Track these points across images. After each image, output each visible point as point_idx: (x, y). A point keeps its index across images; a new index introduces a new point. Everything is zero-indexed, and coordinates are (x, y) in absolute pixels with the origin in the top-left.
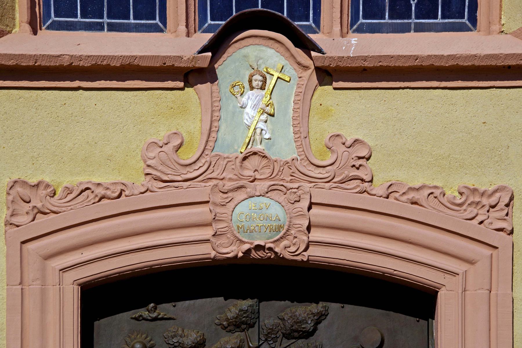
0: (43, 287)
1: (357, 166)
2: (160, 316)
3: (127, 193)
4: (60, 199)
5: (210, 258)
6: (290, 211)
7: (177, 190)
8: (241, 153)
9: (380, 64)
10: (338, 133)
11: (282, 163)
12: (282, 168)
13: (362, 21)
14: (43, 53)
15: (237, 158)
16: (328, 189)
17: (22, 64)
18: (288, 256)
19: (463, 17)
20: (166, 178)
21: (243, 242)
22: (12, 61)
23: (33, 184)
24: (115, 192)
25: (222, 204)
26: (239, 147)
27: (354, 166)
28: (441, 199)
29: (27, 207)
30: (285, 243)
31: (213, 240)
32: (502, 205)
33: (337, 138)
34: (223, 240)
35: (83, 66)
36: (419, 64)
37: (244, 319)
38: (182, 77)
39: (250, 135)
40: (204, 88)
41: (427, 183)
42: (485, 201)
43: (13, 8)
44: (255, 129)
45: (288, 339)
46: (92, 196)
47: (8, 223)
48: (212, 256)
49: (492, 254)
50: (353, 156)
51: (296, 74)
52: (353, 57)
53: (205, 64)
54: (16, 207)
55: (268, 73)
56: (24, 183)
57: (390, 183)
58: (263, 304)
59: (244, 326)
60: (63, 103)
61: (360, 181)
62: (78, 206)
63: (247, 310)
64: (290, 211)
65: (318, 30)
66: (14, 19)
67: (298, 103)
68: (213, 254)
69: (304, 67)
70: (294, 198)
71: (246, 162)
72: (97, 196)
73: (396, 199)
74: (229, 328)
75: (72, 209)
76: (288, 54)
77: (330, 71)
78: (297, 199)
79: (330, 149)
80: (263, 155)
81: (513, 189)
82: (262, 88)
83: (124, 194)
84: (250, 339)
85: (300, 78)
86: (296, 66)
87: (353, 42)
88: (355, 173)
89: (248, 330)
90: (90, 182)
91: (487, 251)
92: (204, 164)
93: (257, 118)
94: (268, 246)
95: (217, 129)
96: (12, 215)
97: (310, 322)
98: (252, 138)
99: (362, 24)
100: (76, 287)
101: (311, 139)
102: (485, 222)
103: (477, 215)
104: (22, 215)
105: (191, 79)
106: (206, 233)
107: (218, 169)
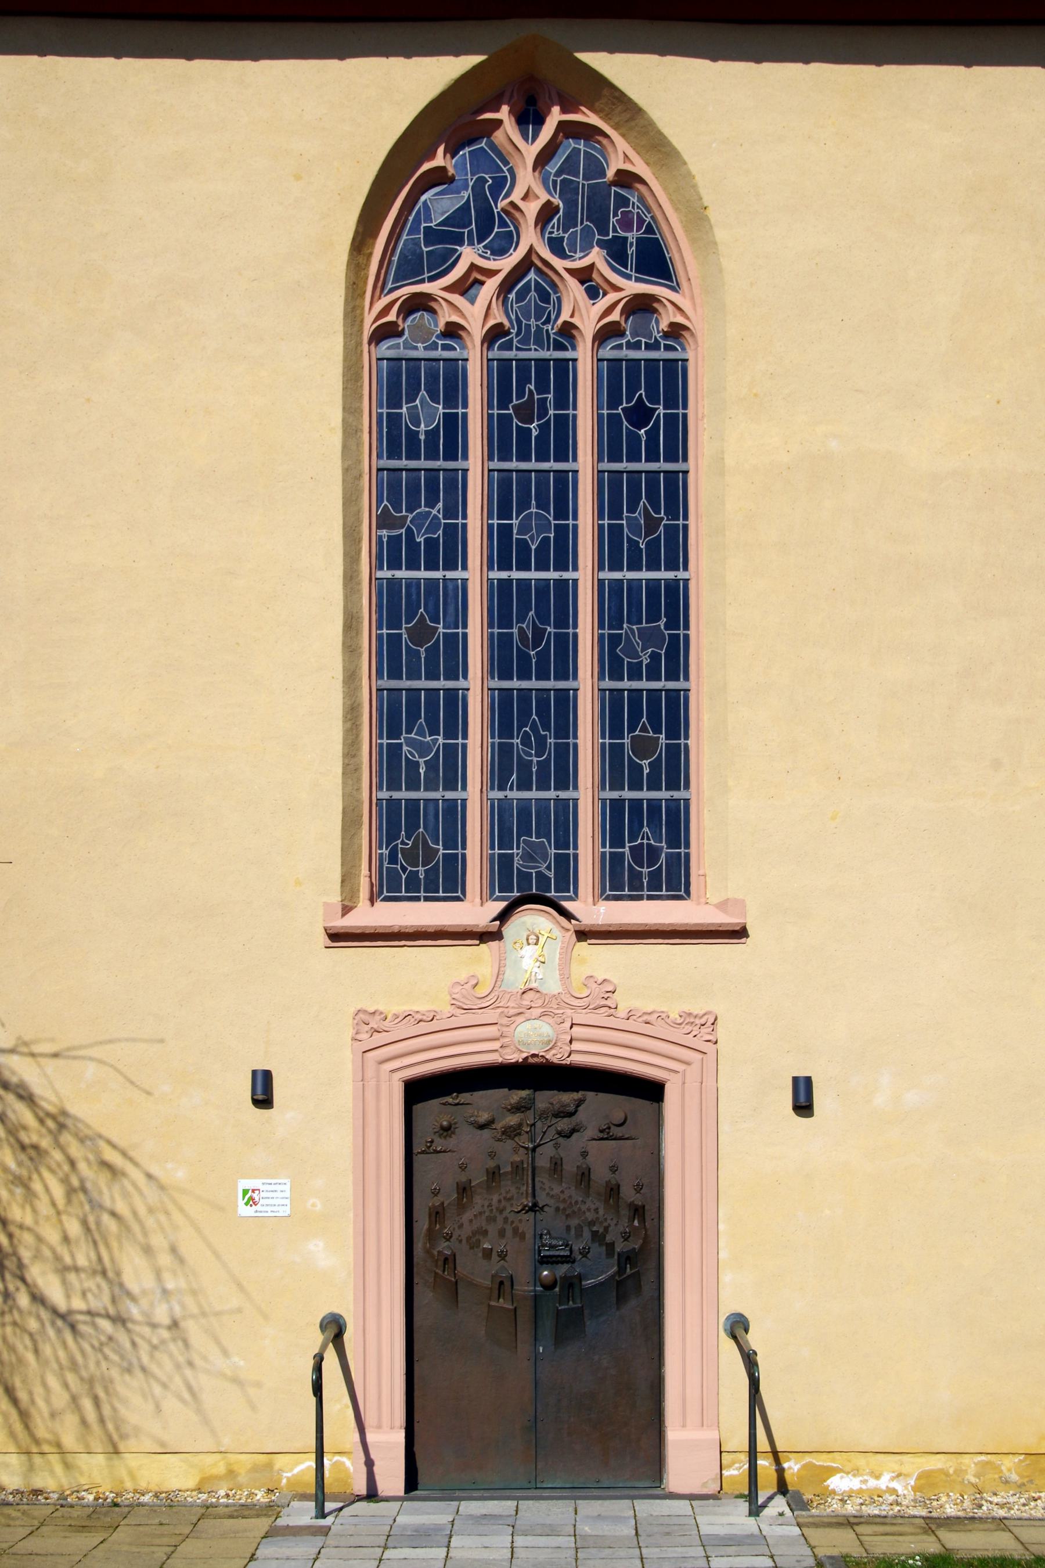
3: (438, 1017)
18: (555, 1061)
20: (466, 1007)
28: (667, 1020)
29: (367, 1028)
30: (553, 1052)
31: (500, 1050)
32: (709, 1024)
34: (507, 1050)
39: (527, 977)
40: (494, 944)
42: (698, 1021)
43: (358, 890)
45: (557, 1118)
46: (413, 1020)
47: (354, 1039)
49: (703, 1058)
53: (495, 929)
56: (365, 1012)
58: (537, 1093)
66: (359, 897)
68: (500, 1060)
70: (560, 1020)
71: (524, 995)
73: (635, 1020)
74: (512, 1111)
76: (554, 921)
81: (717, 1012)
82: (536, 944)
83: (435, 1018)
86: (560, 929)
87: (602, 911)
88: (604, 1002)
91: (699, 1056)
94: (540, 1054)
96: (357, 1034)
99: (609, 895)
100: (401, 1083)
106: (496, 1045)
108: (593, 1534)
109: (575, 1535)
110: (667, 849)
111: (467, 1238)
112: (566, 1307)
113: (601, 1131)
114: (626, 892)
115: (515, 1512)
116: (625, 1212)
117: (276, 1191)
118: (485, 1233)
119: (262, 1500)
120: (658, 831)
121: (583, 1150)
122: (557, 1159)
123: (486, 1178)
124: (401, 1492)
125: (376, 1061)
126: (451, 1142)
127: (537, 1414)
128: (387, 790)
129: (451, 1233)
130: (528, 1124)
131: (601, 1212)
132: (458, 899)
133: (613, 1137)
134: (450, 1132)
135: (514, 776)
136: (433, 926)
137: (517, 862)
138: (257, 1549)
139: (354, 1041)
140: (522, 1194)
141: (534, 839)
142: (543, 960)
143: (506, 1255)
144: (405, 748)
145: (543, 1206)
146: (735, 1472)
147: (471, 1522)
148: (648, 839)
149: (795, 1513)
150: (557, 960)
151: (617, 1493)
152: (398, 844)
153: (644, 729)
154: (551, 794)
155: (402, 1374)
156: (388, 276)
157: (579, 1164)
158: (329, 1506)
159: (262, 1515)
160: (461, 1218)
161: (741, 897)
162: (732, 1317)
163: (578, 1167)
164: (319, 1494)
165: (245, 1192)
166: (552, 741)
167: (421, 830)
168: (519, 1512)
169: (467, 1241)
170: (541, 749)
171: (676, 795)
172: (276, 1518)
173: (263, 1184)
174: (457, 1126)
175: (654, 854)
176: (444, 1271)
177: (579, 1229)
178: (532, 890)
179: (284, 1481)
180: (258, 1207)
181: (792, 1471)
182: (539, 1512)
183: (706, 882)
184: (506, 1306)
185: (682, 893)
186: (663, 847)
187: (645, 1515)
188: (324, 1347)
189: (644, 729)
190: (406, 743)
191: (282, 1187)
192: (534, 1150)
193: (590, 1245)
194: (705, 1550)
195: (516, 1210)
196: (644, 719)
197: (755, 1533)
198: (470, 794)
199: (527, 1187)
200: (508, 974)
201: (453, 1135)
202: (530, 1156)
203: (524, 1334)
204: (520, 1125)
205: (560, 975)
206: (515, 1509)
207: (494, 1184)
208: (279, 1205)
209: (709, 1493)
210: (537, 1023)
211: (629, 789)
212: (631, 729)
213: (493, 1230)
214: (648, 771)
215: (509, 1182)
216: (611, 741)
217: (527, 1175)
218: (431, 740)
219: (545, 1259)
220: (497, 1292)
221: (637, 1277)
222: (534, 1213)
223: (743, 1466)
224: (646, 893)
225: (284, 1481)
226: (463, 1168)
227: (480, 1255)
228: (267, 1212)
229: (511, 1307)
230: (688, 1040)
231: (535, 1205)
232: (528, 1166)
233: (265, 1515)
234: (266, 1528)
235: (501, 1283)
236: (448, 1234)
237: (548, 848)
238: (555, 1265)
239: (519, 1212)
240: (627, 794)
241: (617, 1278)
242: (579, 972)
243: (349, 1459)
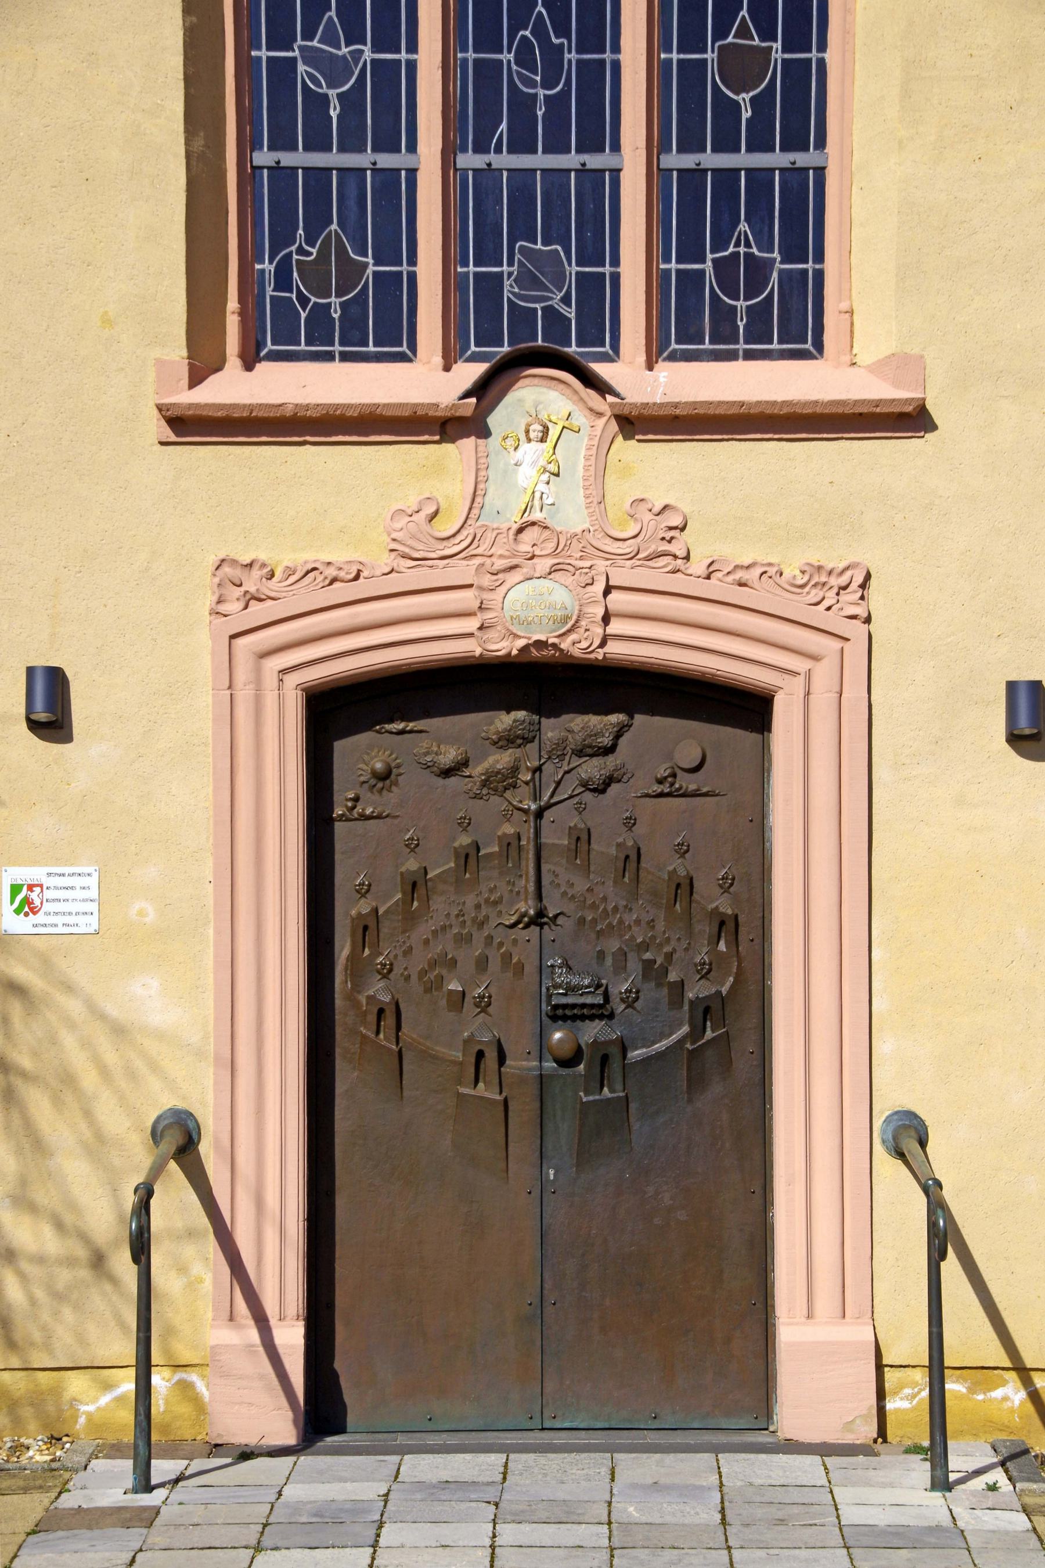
0: (258, 692)
1: (668, 538)
2: (408, 728)
4: (280, 582)
6: (580, 596)
7: (430, 571)
8: (516, 522)
9: (696, 411)
10: (642, 497)
11: (569, 535)
12: (569, 542)
13: (674, 346)
14: (260, 401)
15: (509, 529)
16: (630, 567)
17: (235, 415)
18: (576, 652)
19: (806, 342)
21: (517, 636)
22: (222, 412)
23: (245, 563)
24: (350, 573)
25: (491, 588)
26: (512, 516)
27: (663, 539)
29: (238, 592)
30: (573, 637)
32: (854, 585)
33: (641, 503)
34: (491, 634)
35: (310, 417)
36: (746, 411)
37: (520, 732)
38: (437, 428)
41: (759, 559)
42: (835, 582)
45: (580, 757)
48: (477, 653)
49: (842, 648)
50: (663, 526)
51: (587, 423)
52: (660, 403)
53: (468, 412)
54: (224, 591)
55: (550, 421)
56: (234, 562)
57: (710, 560)
59: (519, 741)
60: (284, 461)
61: (671, 557)
62: (302, 591)
63: (524, 721)
64: (580, 596)
65: (616, 358)
67: (589, 459)
68: (478, 651)
69: (597, 413)
72: (326, 578)
74: (500, 743)
75: (294, 595)
76: (575, 398)
77: (633, 420)
78: (590, 581)
79: (632, 517)
80: (545, 525)
81: (869, 565)
82: (543, 440)
83: (362, 575)
84: (528, 757)
85: (592, 427)
86: (587, 413)
87: (662, 380)
88: (665, 547)
89: (525, 746)
90: (318, 560)
92: (467, 537)
94: (550, 641)
95: (483, 492)
96: (219, 602)
97: (607, 735)
98: (530, 504)
99: (675, 351)
100: (300, 693)
101: (606, 505)
103: (823, 598)
104: (232, 601)
105: (449, 428)
106: (471, 625)
107: (485, 543)
108: (644, 1519)
109: (610, 1523)
110: (781, 263)
111: (420, 973)
112: (597, 1097)
113: (660, 782)
114: (707, 346)
115: (501, 1476)
116: (704, 928)
118: (453, 963)
119: (38, 1458)
120: (766, 229)
121: (628, 814)
122: (581, 830)
123: (452, 865)
124: (289, 1437)
125: (254, 653)
126: (389, 801)
127: (545, 1292)
128: (270, 149)
129: (391, 964)
130: (528, 768)
131: (660, 926)
132: (402, 358)
133: (681, 792)
134: (388, 782)
135: (504, 126)
136: (356, 406)
137: (509, 288)
138: (15, 1556)
139: (214, 616)
140: (518, 893)
141: (539, 246)
142: (555, 470)
143: (489, 1004)
144: (301, 68)
145: (556, 916)
146: (905, 1405)
147: (418, 1496)
148: (748, 245)
149: (1019, 1485)
150: (580, 471)
151: (691, 1438)
152: (292, 252)
153: (743, 32)
154: (571, 160)
157: (620, 840)
158: (162, 1468)
159: (35, 1488)
160: (409, 937)
161: (916, 351)
162: (896, 1117)
163: (619, 845)
164: (141, 1443)
165: (15, 889)
166: (573, 56)
167: (334, 227)
168: (508, 1477)
169: (420, 978)
170: (553, 73)
171: (801, 159)
172: (60, 1493)
173: (49, 874)
174: (401, 771)
175: (758, 271)
176: (378, 1033)
177: (622, 955)
178: (537, 341)
179: (82, 1420)
180: (40, 918)
181: (1009, 1404)
182: (545, 1475)
183: (852, 324)
184: (487, 1095)
185: (809, 346)
186: (775, 260)
187: (739, 1483)
188: (157, 1171)
189: (743, 32)
190: (302, 57)
192: (539, 814)
193: (639, 985)
194: (849, 1555)
195: (507, 923)
196: (744, 12)
197: (944, 1524)
198: (422, 159)
199: (527, 881)
200: (493, 498)
201: (394, 788)
202: (532, 824)
203: (522, 1145)
204: (515, 770)
206: (502, 1469)
207: (468, 875)
208: (77, 914)
209: (858, 1442)
211: (714, 150)
212: (721, 32)
213: (467, 957)
214: (750, 113)
215: (495, 873)
216: (682, 56)
217: (527, 859)
218: (350, 52)
219: (560, 1012)
220: (472, 1070)
221: (724, 1041)
222: (538, 928)
223: (919, 1393)
224: (742, 346)
225: (82, 1420)
226: (413, 846)
227: (443, 1002)
228: (56, 925)
229: (498, 1097)
230: (817, 616)
231: (541, 913)
232: (528, 842)
233: (41, 1487)
234: (38, 1514)
235: (480, 1055)
236: (385, 965)
238: (579, 1023)
239: (513, 926)
240: (711, 159)
241: (689, 1046)
243: (203, 1377)
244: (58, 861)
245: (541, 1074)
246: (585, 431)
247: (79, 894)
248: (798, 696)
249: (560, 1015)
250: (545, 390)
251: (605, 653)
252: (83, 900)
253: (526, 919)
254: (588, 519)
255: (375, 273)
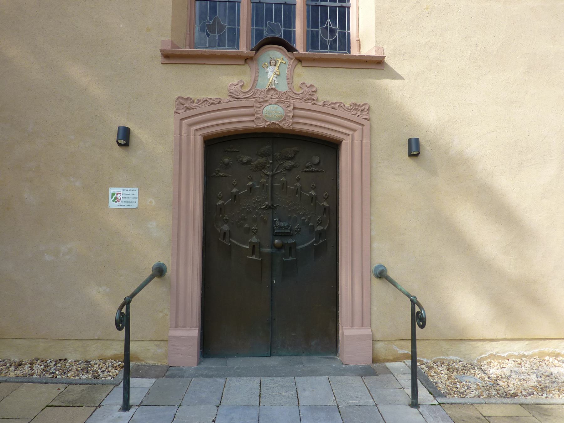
5: (254, 128)
18: (284, 127)
20: (237, 97)
27: (310, 94)
29: (183, 107)
44: (272, 80)
47: (176, 112)
56: (182, 98)
68: (255, 126)
70: (287, 105)
78: (288, 106)
82: (275, 66)
88: (310, 97)
91: (361, 127)
92: (252, 92)
93: (273, 76)
94: (277, 123)
98: (271, 83)
102: (360, 116)
104: (181, 109)
106: (253, 118)
117: (130, 194)
120: (335, 21)
125: (187, 125)
141: (273, 23)
148: (330, 25)
155: (198, 297)
156: (229, 54)
165: (113, 194)
173: (123, 190)
180: (120, 203)
191: (134, 192)
192: (273, 176)
200: (260, 81)
205: (287, 82)
208: (131, 202)
210: (275, 106)
219: (277, 234)
228: (125, 206)
230: (355, 118)
237: (281, 27)
242: (298, 81)
244: (126, 186)
245: (272, 252)
246: (288, 63)
247: (132, 196)
248: (349, 142)
249: (276, 235)
250: (275, 52)
251: (293, 128)
252: (133, 198)
253: (268, 207)
254: (288, 88)
255: (228, 28)
